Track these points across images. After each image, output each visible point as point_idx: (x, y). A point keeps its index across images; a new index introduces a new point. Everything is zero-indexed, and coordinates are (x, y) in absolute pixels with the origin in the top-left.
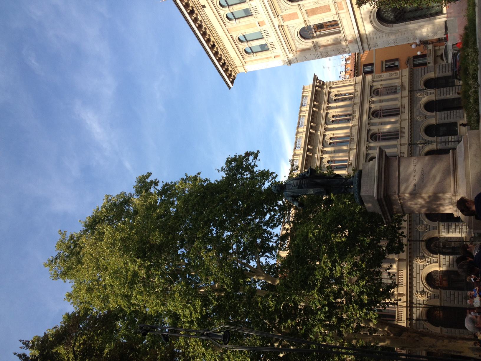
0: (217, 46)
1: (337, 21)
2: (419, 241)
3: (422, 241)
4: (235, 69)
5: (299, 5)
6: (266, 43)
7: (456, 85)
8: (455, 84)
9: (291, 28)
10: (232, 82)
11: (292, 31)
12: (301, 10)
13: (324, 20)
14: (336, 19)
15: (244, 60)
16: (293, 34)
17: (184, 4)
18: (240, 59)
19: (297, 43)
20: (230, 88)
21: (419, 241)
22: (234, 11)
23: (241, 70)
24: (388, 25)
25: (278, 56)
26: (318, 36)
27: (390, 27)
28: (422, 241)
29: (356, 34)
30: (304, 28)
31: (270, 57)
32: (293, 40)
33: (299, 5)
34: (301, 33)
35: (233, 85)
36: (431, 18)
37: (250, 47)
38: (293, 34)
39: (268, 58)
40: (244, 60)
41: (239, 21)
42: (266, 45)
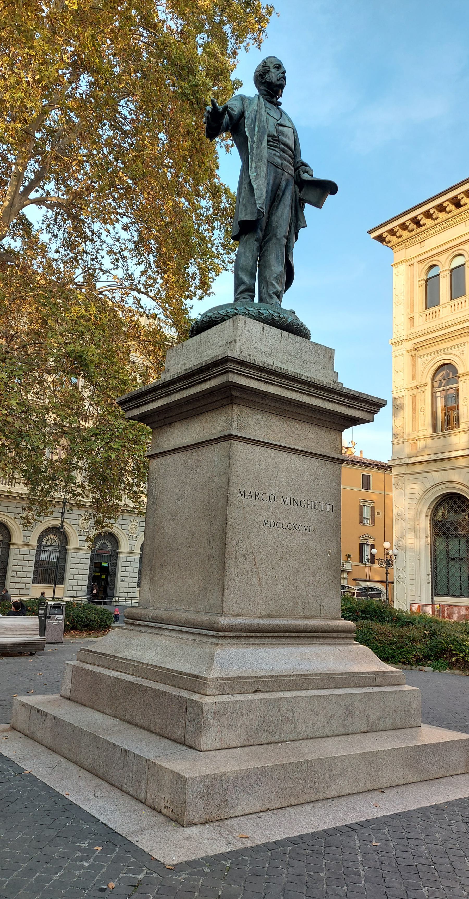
0: (418, 230)
1: (459, 427)
2: (63, 518)
3: (62, 521)
4: (404, 245)
5: (425, 385)
6: (441, 303)
7: (57, 586)
8: (59, 584)
9: (461, 349)
10: (380, 239)
11: (455, 351)
12: (418, 388)
13: (464, 406)
14: (461, 426)
15: (416, 264)
16: (450, 351)
17: (445, 204)
18: (420, 255)
19: (430, 358)
20: (370, 232)
21: (63, 518)
22: (441, 279)
23: (401, 254)
24: (430, 509)
25: (412, 325)
26: (434, 394)
27: (427, 513)
28: (62, 521)
29: (446, 454)
30: (457, 372)
31: (412, 311)
32: (437, 351)
33: (425, 385)
34: (446, 366)
35: (374, 238)
36: (430, 576)
37: (439, 275)
38: (450, 351)
39: (412, 305)
40: (416, 264)
41: (420, 286)
42: (438, 304)
